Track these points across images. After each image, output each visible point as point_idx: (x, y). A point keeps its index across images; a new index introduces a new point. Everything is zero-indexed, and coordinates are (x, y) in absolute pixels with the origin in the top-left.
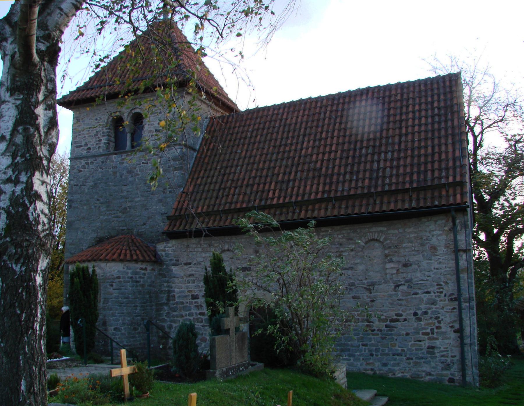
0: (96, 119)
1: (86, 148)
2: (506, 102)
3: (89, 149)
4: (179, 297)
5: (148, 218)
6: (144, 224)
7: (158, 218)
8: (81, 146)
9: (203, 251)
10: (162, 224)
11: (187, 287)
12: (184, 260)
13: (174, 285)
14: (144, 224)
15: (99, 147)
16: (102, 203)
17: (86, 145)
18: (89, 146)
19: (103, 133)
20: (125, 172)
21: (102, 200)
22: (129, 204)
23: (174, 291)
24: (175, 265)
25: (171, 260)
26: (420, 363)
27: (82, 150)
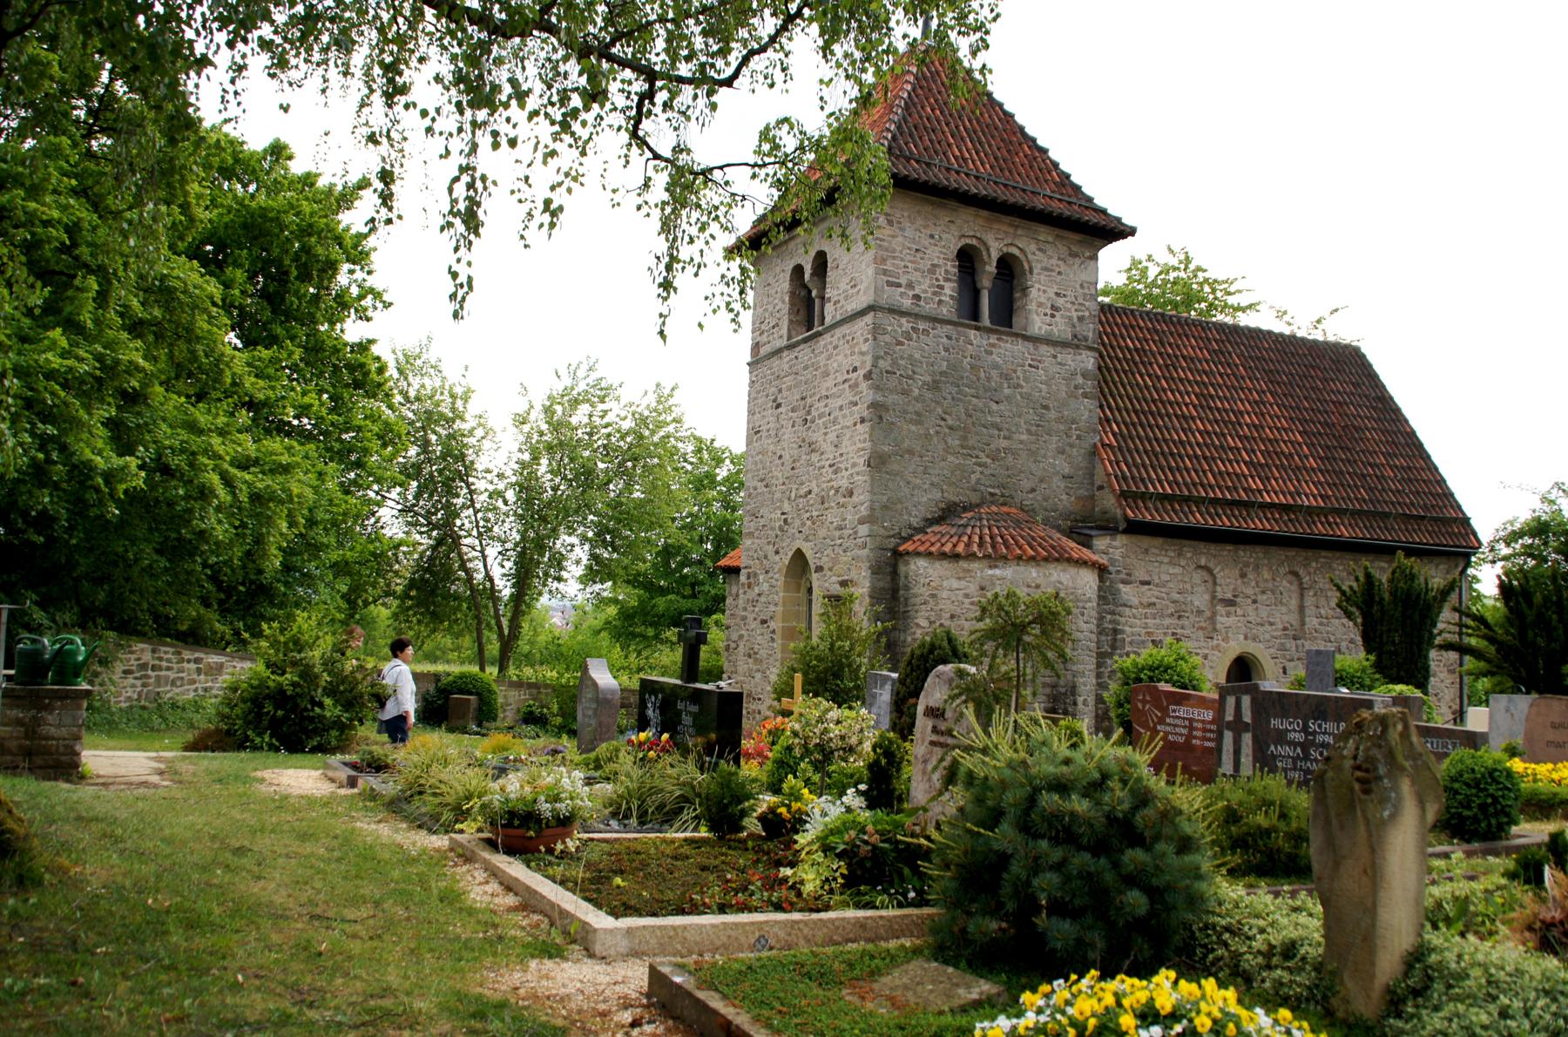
0: (932, 236)
1: (911, 293)
2: (379, 287)
3: (917, 297)
4: (1131, 643)
5: (1042, 481)
6: (1033, 490)
7: (1057, 482)
8: (899, 285)
9: (1170, 563)
10: (1064, 497)
11: (1146, 626)
12: (1141, 574)
13: (1123, 620)
14: (1033, 490)
15: (940, 302)
16: (950, 428)
17: (910, 286)
18: (917, 291)
19: (947, 272)
20: (994, 373)
21: (950, 422)
22: (1004, 443)
23: (1122, 632)
24: (1124, 582)
25: (1118, 572)
26: (232, 464)
27: (902, 294)
